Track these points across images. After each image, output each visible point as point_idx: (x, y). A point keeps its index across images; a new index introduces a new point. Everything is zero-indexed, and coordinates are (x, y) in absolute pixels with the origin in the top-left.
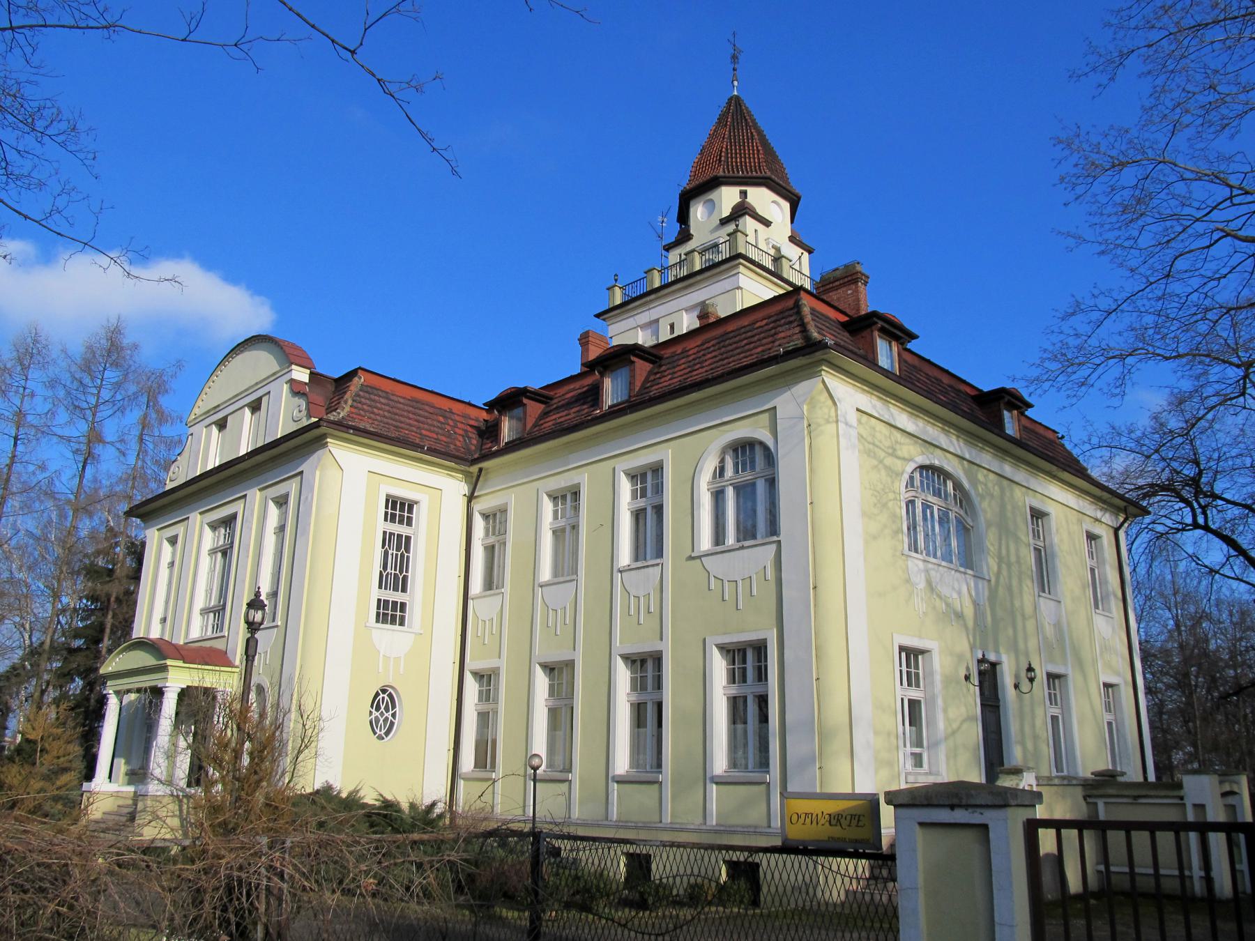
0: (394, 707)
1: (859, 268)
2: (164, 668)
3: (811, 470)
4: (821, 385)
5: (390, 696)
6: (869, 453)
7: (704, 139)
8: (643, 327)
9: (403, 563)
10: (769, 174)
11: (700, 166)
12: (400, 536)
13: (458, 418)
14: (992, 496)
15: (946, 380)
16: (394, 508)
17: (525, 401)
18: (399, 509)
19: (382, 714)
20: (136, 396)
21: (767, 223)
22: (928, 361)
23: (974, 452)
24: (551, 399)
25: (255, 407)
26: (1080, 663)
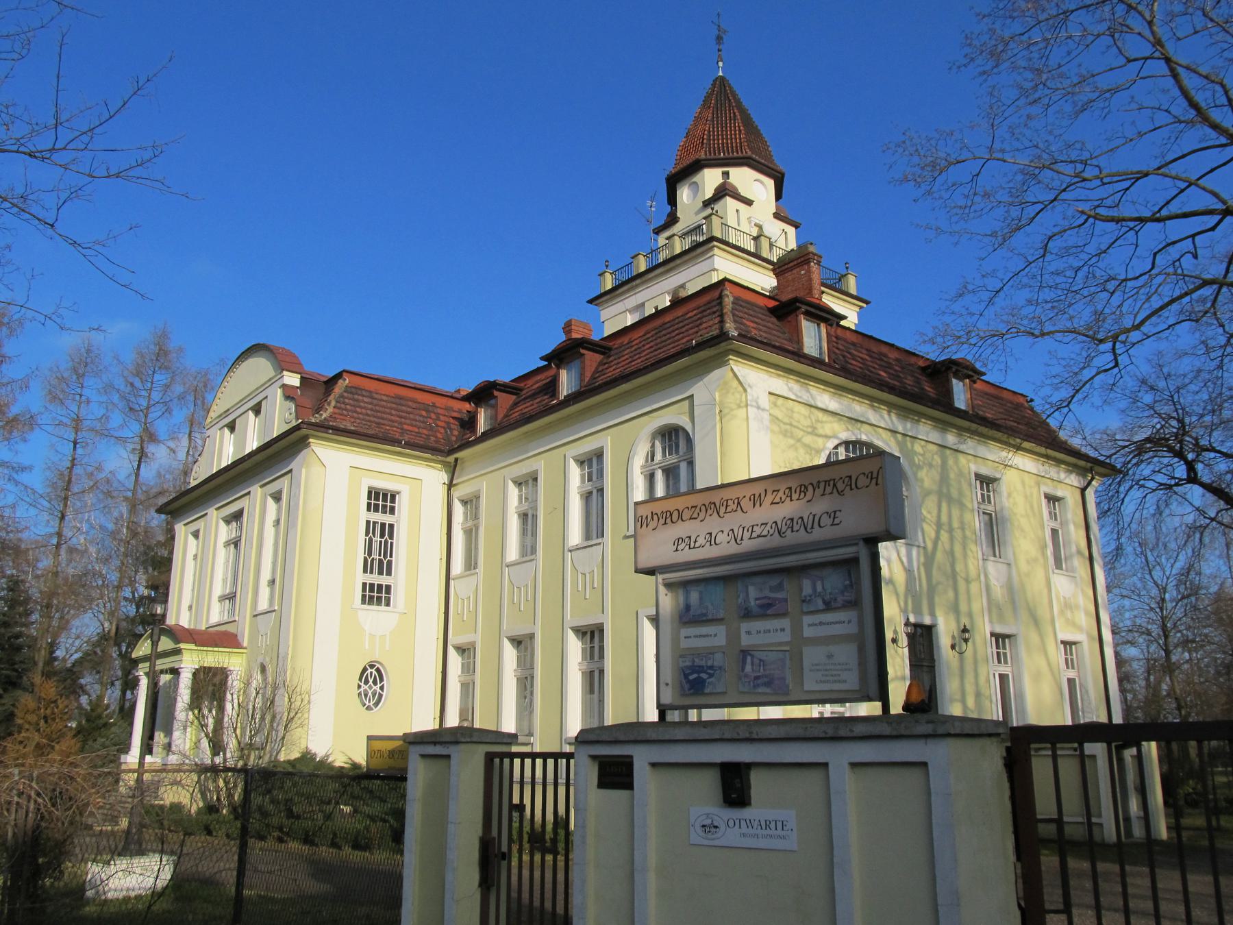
0: (382, 680)
1: (812, 249)
2: (178, 652)
3: (722, 453)
4: (731, 374)
5: (378, 670)
6: (785, 434)
7: (689, 122)
8: (631, 311)
9: (387, 550)
10: (749, 153)
11: (685, 149)
12: (383, 525)
13: (439, 411)
14: (931, 466)
15: (893, 355)
16: (377, 498)
17: (496, 393)
18: (381, 500)
19: (370, 687)
20: (181, 397)
21: (749, 202)
22: (871, 337)
23: (909, 425)
24: (521, 390)
25: (257, 410)
26: (1036, 621)
